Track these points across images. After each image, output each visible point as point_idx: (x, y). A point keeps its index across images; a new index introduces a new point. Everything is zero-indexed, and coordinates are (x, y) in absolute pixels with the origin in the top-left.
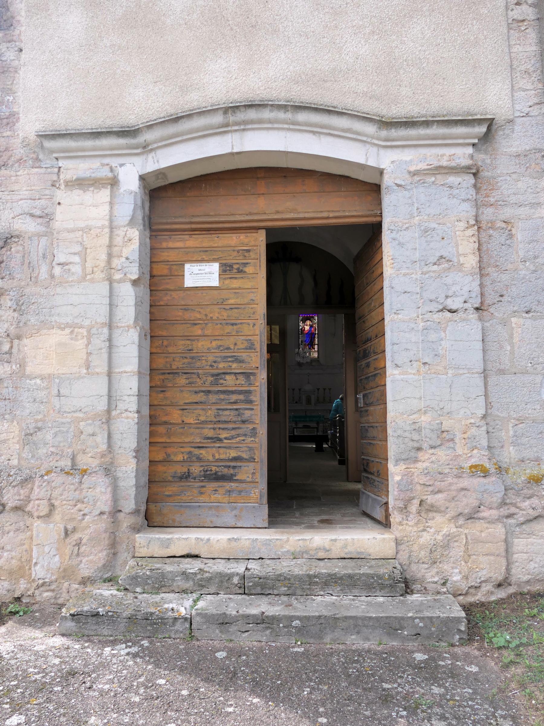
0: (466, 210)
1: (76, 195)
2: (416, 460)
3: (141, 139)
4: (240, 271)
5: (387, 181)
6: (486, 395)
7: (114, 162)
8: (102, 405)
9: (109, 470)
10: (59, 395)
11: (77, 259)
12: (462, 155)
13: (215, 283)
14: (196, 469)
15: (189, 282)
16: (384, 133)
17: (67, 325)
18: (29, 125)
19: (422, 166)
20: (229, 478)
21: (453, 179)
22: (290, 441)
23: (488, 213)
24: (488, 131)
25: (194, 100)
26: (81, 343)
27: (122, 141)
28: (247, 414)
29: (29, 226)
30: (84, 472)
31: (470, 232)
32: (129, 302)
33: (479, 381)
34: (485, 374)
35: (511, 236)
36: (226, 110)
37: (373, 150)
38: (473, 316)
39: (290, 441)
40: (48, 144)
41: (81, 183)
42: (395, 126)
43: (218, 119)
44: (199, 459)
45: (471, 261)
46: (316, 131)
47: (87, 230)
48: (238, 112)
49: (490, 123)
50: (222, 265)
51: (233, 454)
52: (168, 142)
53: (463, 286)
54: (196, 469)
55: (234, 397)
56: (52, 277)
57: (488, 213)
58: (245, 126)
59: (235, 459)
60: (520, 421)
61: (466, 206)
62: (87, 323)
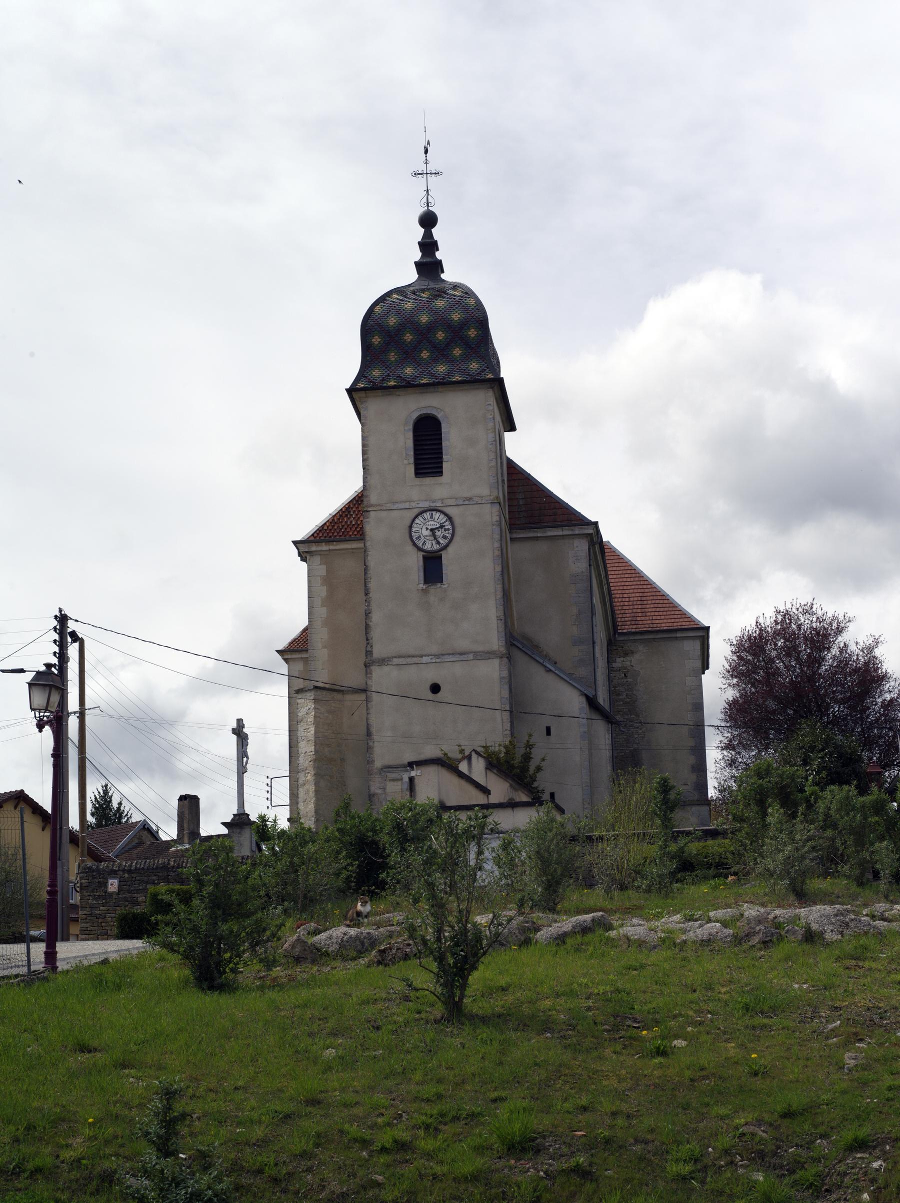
1: (392, 783)
18: (378, 764)
25: (422, 757)
29: (380, 791)
41: (393, 780)
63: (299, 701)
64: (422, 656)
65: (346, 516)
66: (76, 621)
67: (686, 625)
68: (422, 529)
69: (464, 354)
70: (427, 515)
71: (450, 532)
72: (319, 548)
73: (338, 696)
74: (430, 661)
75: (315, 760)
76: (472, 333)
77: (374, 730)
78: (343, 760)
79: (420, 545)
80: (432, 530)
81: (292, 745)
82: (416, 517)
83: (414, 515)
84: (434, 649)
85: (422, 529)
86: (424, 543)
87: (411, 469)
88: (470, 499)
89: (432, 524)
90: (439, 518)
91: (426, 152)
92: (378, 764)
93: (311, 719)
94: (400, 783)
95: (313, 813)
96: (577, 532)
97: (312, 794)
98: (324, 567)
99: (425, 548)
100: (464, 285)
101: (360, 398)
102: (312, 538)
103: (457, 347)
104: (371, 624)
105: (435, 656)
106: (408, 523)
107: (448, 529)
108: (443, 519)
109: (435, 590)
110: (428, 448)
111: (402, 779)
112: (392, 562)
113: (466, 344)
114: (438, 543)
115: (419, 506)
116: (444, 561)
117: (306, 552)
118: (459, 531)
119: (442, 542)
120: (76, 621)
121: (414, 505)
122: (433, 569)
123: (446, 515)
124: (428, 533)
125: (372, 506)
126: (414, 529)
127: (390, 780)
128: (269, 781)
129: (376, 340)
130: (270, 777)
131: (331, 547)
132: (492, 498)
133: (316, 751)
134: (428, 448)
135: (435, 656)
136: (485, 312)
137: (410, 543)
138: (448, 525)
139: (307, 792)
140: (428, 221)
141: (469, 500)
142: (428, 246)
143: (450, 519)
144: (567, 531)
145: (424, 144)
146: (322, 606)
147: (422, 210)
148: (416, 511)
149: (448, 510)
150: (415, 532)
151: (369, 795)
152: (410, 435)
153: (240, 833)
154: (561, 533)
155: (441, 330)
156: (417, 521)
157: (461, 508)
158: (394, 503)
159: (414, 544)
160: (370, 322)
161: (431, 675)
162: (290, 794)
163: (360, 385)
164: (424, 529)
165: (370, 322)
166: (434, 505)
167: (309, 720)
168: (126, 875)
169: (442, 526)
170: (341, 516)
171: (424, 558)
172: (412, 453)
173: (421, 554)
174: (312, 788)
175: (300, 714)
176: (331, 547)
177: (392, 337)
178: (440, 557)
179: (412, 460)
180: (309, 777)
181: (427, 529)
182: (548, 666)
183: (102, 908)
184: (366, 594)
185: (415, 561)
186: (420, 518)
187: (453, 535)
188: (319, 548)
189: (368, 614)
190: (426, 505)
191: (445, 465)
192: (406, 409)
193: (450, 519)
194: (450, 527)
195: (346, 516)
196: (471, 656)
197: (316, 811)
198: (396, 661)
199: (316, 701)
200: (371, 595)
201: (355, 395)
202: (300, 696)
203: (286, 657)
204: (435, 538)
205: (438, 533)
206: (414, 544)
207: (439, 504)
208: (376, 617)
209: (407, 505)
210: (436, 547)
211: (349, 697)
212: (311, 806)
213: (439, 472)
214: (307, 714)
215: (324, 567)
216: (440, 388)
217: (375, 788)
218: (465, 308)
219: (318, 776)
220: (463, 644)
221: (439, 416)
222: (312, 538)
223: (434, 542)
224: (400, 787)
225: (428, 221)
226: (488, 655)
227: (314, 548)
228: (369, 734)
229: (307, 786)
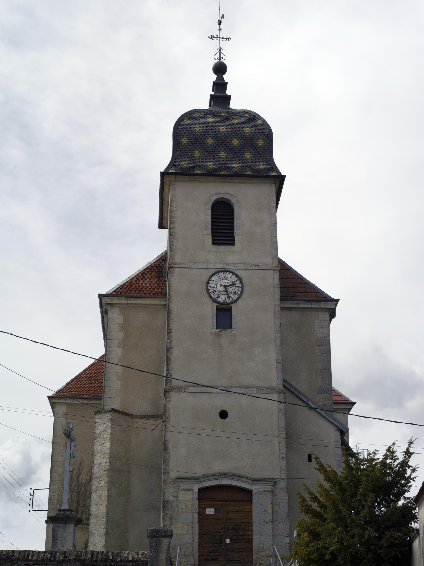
0: (270, 500)
1: (184, 492)
2: (258, 554)
3: (199, 480)
4: (219, 511)
5: (253, 493)
6: (273, 541)
7: (192, 485)
8: (191, 541)
9: (193, 555)
10: (181, 538)
11: (184, 507)
12: (269, 488)
13: (213, 513)
14: (209, 557)
15: (207, 513)
16: (253, 482)
17: (183, 522)
18: (173, 475)
19: (261, 490)
20: (217, 560)
21: (267, 493)
22: (229, 240)
23: (274, 501)
24: (274, 482)
25: (211, 472)
26: (186, 527)
27: (195, 481)
28: (221, 545)
29: (173, 499)
30: (188, 555)
31: (271, 505)
32: (196, 516)
33: (272, 537)
34: (273, 536)
35: (279, 506)
36: (219, 475)
37: (250, 485)
38: (271, 523)
39: (229, 240)
40: (178, 480)
41: (186, 490)
42: (255, 481)
43: (217, 477)
44: (210, 555)
45: (271, 511)
46: (238, 480)
47: (187, 501)
48: (221, 475)
49: (275, 482)
50: (215, 509)
51: (218, 554)
52: (205, 481)
53: (269, 517)
54: (209, 557)
55: (218, 541)
56: (179, 511)
57: (274, 501)
58: (222, 478)
59: (218, 555)
60: (280, 546)
61: (270, 499)
62: (187, 522)
63: (97, 421)
65: (142, 279)
67: (340, 400)
68: (217, 285)
69: (254, 157)
70: (222, 275)
71: (240, 289)
72: (120, 302)
73: (128, 419)
75: (109, 470)
76: (260, 143)
77: (170, 445)
78: (129, 472)
80: (225, 286)
82: (213, 275)
83: (211, 274)
84: (223, 382)
85: (217, 285)
86: (218, 297)
87: (209, 239)
89: (225, 282)
91: (220, 23)
92: (173, 475)
93: (107, 435)
94: (191, 493)
95: (104, 515)
96: (323, 306)
97: (104, 498)
98: (122, 317)
100: (251, 111)
101: (170, 181)
102: (114, 293)
103: (248, 151)
104: (171, 357)
106: (206, 280)
107: (238, 287)
109: (225, 334)
110: (223, 224)
111: (193, 490)
112: (189, 309)
113: (255, 149)
114: (229, 297)
115: (216, 267)
116: (234, 312)
117: (109, 304)
118: (247, 290)
119: (233, 296)
121: (211, 266)
122: (224, 315)
123: (237, 276)
124: (222, 288)
126: (210, 285)
127: (183, 490)
129: (185, 140)
130: (33, 489)
132: (274, 266)
133: (110, 463)
134: (223, 224)
136: (270, 129)
138: (238, 284)
139: (100, 497)
140: (220, 69)
141: (255, 267)
142: (220, 86)
143: (240, 279)
144: (315, 305)
145: (219, 18)
146: (118, 347)
147: (214, 62)
148: (213, 271)
149: (238, 272)
150: (211, 287)
151: (164, 502)
152: (209, 212)
153: (64, 528)
154: (310, 306)
155: (235, 138)
156: (213, 278)
157: (249, 272)
158: (195, 263)
159: (210, 297)
160: (180, 128)
161: (221, 402)
162: (49, 501)
163: (171, 171)
164: (219, 286)
165: (180, 128)
166: (227, 267)
167: (107, 436)
169: (233, 284)
171: (218, 309)
173: (215, 305)
174: (105, 493)
175: (97, 431)
176: (129, 302)
177: (197, 140)
178: (230, 310)
179: (210, 232)
180: (102, 484)
181: (221, 285)
184: (168, 333)
185: (210, 310)
188: (120, 302)
189: (169, 349)
190: (221, 266)
191: (236, 238)
192: (208, 192)
193: (240, 279)
194: (240, 285)
195: (142, 279)
196: (254, 390)
197: (107, 514)
198: (192, 389)
199: (112, 420)
200: (172, 334)
201: (167, 179)
202: (98, 416)
203: (54, 401)
204: (228, 294)
205: (230, 290)
206: (210, 297)
207: (231, 267)
208: (176, 352)
209: (205, 266)
210: (227, 300)
211: (136, 420)
212: (103, 509)
213: (232, 243)
214: (104, 431)
215: (122, 317)
216: (235, 180)
217: (169, 496)
218: (255, 126)
219: (111, 484)
220: (249, 380)
221: (233, 200)
222: (114, 293)
223: (226, 296)
224: (191, 496)
225: (220, 69)
226: (270, 390)
227: (115, 301)
228: (166, 449)
229: (100, 492)
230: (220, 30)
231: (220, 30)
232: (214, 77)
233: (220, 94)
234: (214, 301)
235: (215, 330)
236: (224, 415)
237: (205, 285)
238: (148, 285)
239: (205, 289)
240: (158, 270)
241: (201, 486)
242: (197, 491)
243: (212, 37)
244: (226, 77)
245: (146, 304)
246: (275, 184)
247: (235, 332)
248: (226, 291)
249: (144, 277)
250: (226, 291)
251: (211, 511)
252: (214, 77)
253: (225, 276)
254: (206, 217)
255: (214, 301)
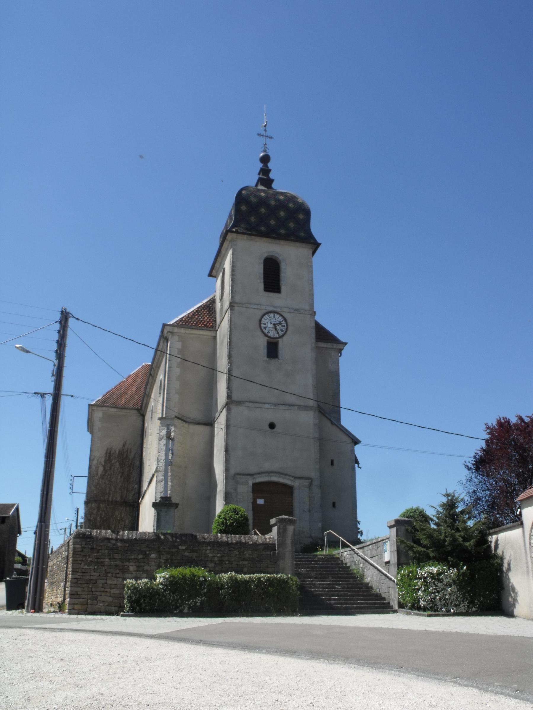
29: (232, 491)
32: (251, 505)
45: (308, 503)
64: (264, 403)
66: (78, 319)
68: (268, 323)
70: (272, 315)
74: (269, 407)
76: (301, 216)
79: (266, 333)
80: (274, 324)
81: (92, 459)
85: (268, 323)
86: (269, 332)
88: (298, 310)
90: (279, 318)
96: (335, 347)
99: (269, 335)
105: (273, 404)
106: (259, 317)
107: (284, 326)
108: (280, 319)
109: (273, 362)
110: (272, 276)
114: (278, 333)
116: (280, 345)
118: (290, 328)
120: (78, 319)
121: (263, 307)
123: (283, 317)
124: (272, 326)
125: (236, 303)
126: (262, 322)
128: (72, 478)
129: (244, 208)
131: (187, 332)
134: (272, 276)
135: (273, 404)
137: (260, 330)
140: (265, 159)
142: (265, 171)
143: (285, 320)
148: (264, 311)
149: (284, 314)
152: (262, 266)
156: (265, 317)
161: (270, 415)
166: (275, 310)
168: (119, 544)
169: (280, 323)
170: (193, 314)
172: (262, 276)
176: (187, 332)
179: (262, 281)
181: (271, 323)
182: (334, 421)
183: (93, 574)
185: (262, 342)
186: (267, 316)
187: (287, 330)
190: (271, 309)
192: (265, 247)
193: (285, 320)
194: (285, 325)
205: (278, 327)
209: (259, 307)
210: (276, 335)
227: (176, 330)
230: (265, 130)
231: (265, 130)
232: (261, 165)
233: (265, 179)
234: (266, 335)
235: (266, 358)
236: (272, 426)
237: (258, 322)
238: (201, 319)
239: (258, 325)
240: (209, 310)
241: (254, 482)
242: (251, 485)
243: (259, 135)
244: (270, 165)
245: (200, 335)
246: (312, 248)
247: (281, 361)
248: (276, 329)
249: (198, 313)
250: (276, 329)
251: (260, 501)
252: (261, 165)
253: (274, 317)
254: (259, 269)
255: (266, 335)
